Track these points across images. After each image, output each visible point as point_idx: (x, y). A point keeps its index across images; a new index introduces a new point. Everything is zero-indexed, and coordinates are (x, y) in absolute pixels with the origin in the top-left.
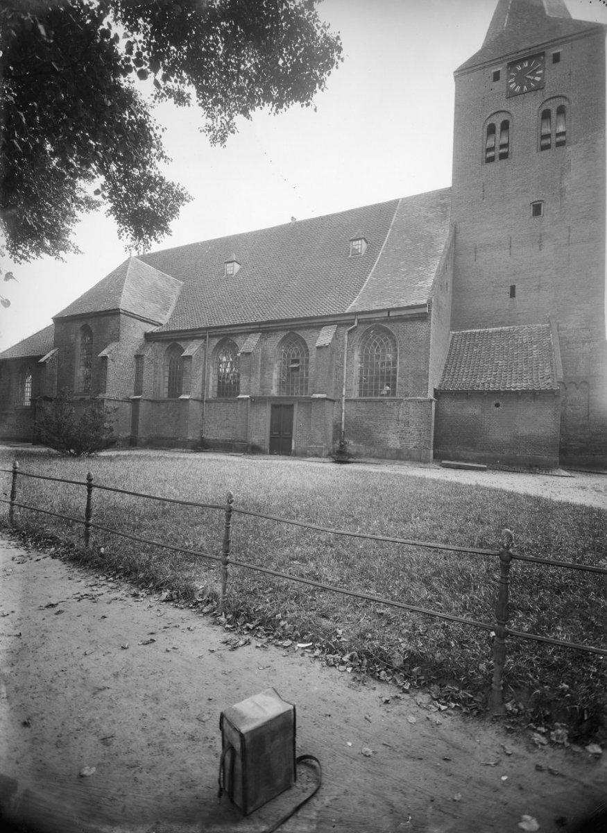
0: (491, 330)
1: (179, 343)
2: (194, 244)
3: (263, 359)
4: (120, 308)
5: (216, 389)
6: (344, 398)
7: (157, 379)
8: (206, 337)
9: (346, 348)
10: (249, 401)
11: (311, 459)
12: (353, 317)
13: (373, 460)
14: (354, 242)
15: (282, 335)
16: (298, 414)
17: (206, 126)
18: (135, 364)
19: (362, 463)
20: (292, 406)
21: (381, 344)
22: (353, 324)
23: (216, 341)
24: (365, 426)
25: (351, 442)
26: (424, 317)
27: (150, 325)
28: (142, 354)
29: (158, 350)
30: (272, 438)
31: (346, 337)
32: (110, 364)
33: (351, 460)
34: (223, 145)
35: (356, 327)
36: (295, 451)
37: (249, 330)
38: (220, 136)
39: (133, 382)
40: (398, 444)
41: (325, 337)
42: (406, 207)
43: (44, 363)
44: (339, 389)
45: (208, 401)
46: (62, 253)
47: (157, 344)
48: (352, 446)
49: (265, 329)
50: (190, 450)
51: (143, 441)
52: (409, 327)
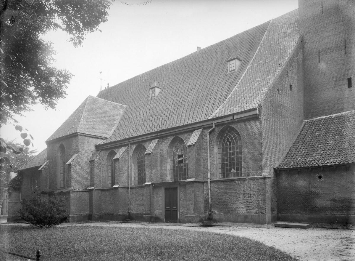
0: (334, 115)
1: (114, 150)
2: (137, 76)
3: (161, 156)
4: (78, 132)
5: (137, 179)
6: (209, 180)
7: (104, 175)
8: (128, 144)
9: (208, 144)
10: (151, 187)
11: (187, 224)
12: (211, 122)
13: (229, 224)
14: (230, 62)
15: (171, 138)
16: (180, 193)
17: (70, 38)
18: (90, 166)
19: (219, 226)
20: (176, 188)
21: (228, 139)
22: (212, 127)
23: (134, 147)
24: (224, 199)
25: (216, 211)
26: (256, 118)
27: (99, 140)
28: (93, 159)
29: (104, 154)
30: (166, 211)
31: (208, 136)
32: (73, 168)
33: (215, 224)
34: (81, 46)
35: (214, 129)
36: (179, 219)
37: (152, 138)
38: (79, 41)
39: (89, 178)
40: (245, 211)
41: (193, 139)
42: (274, 26)
43: (41, 170)
44: (206, 174)
45: (131, 188)
46: (22, 113)
47: (103, 152)
48: (216, 214)
49: (161, 135)
50: (120, 222)
51: (96, 216)
52: (247, 126)
